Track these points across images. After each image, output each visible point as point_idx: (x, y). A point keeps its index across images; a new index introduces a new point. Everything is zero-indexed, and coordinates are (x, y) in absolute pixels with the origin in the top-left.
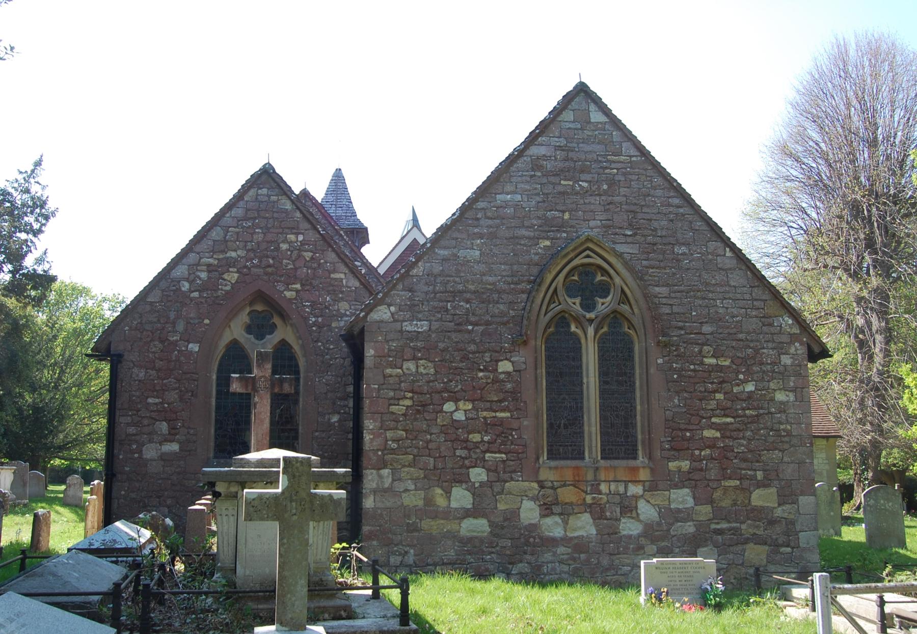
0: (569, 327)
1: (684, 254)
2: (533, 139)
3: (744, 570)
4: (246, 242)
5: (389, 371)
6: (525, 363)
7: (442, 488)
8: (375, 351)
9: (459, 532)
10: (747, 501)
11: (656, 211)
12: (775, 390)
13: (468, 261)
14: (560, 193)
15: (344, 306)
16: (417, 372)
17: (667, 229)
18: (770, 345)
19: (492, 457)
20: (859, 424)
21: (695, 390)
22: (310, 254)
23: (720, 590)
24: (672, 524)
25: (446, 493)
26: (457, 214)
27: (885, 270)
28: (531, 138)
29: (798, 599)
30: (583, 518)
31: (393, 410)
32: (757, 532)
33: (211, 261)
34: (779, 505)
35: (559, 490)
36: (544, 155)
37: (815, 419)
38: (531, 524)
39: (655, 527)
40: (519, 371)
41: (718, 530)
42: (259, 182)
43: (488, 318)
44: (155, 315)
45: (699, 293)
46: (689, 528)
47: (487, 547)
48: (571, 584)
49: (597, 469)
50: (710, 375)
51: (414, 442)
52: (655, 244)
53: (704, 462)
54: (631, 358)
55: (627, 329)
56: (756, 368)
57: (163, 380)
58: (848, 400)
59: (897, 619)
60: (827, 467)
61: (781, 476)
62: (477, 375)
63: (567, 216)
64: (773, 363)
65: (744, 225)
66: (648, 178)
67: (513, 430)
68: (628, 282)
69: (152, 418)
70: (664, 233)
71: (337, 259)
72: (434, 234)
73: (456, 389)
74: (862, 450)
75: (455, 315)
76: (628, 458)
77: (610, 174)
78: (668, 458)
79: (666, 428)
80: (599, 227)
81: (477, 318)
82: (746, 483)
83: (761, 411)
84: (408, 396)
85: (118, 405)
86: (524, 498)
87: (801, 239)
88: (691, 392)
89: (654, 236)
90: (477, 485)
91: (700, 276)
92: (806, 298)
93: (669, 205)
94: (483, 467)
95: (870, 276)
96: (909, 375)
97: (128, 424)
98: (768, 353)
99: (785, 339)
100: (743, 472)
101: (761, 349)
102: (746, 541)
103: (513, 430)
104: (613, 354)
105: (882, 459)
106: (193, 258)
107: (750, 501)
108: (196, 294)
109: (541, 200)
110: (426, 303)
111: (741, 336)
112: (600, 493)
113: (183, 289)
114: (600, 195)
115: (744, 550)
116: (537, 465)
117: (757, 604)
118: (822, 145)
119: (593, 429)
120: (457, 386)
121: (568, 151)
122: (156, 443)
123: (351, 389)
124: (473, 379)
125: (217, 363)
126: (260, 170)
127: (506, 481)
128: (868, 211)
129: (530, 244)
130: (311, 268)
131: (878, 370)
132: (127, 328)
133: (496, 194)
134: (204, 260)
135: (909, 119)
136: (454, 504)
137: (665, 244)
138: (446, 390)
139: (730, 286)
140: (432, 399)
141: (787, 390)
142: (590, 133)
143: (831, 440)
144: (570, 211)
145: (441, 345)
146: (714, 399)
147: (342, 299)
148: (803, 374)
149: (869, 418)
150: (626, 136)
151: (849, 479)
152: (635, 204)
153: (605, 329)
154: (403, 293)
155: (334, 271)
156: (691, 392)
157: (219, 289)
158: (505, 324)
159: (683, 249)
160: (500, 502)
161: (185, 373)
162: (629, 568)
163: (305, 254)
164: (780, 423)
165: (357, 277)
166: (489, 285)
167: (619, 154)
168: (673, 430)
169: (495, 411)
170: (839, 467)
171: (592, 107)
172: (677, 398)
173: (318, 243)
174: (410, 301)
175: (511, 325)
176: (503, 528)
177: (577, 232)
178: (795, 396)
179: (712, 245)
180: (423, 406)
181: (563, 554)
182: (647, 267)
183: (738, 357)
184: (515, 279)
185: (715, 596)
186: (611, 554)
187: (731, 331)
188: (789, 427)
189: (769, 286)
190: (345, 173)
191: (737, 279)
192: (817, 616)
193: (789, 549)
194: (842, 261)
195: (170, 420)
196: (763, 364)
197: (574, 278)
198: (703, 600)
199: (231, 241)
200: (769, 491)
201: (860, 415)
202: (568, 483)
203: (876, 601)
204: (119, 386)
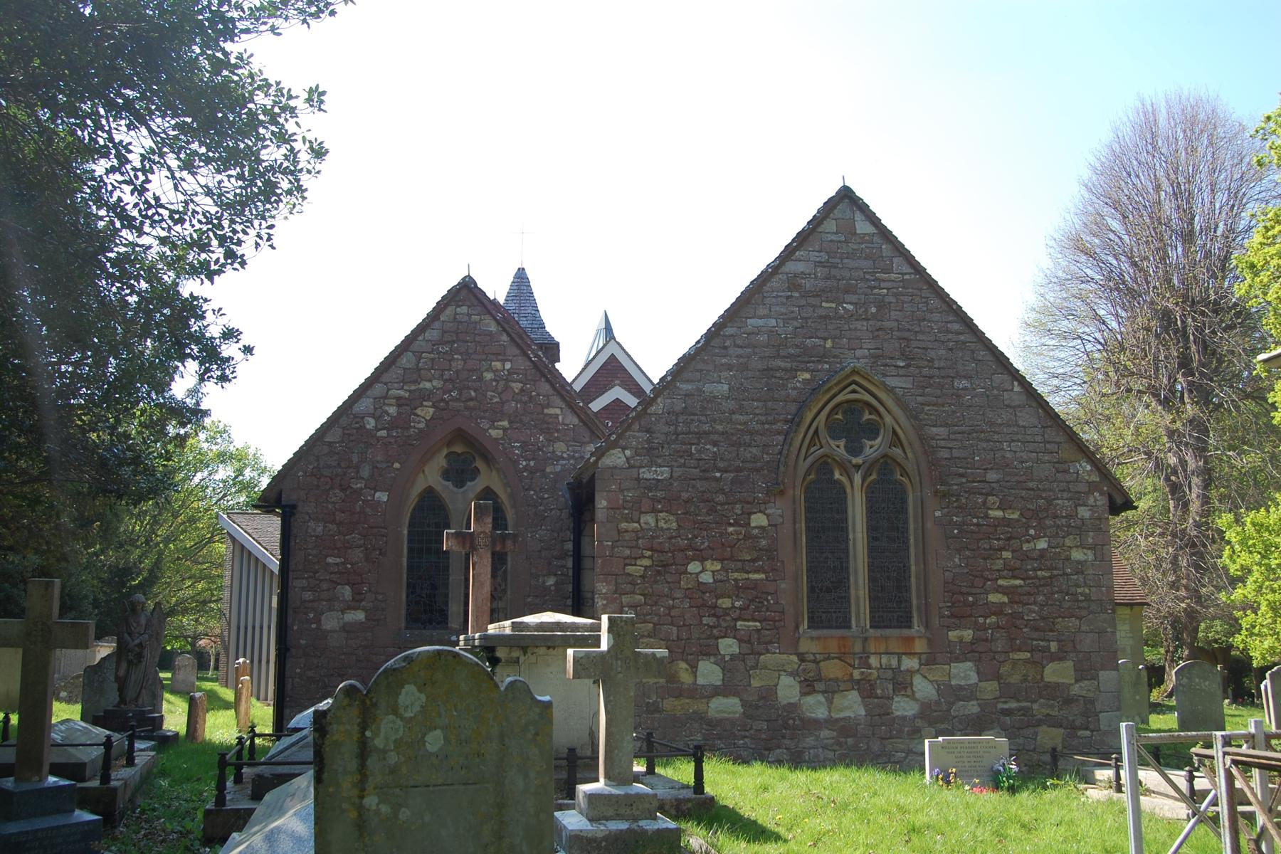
0: (832, 474)
1: (965, 389)
2: (790, 252)
3: (1035, 757)
4: (443, 370)
5: (624, 525)
6: (782, 516)
7: (687, 662)
8: (608, 502)
9: (707, 713)
10: (1039, 677)
11: (933, 338)
12: (1071, 548)
13: (714, 397)
14: (821, 317)
15: (560, 447)
16: (657, 526)
17: (946, 359)
18: (1065, 495)
19: (745, 625)
20: (1171, 588)
21: (978, 548)
22: (520, 385)
23: (1013, 771)
24: (953, 703)
25: (692, 667)
26: (702, 342)
27: (1203, 396)
28: (786, 253)
29: (1101, 781)
30: (850, 697)
31: (629, 571)
32: (1051, 713)
33: (401, 393)
34: (1077, 681)
35: (822, 664)
36: (802, 273)
37: (1118, 582)
38: (790, 704)
39: (933, 707)
40: (775, 525)
41: (1007, 709)
42: (457, 299)
43: (739, 463)
44: (334, 458)
45: (983, 435)
46: (973, 708)
47: (739, 731)
48: (847, 766)
49: (866, 640)
50: (996, 530)
51: (654, 609)
52: (931, 377)
53: (990, 631)
54: (904, 510)
55: (899, 477)
56: (1049, 522)
57: (344, 536)
58: (1157, 559)
59: (1196, 758)
60: (1131, 642)
61: (1078, 647)
62: (726, 529)
63: (829, 344)
64: (1069, 517)
65: (1027, 338)
66: (924, 300)
67: (768, 593)
68: (900, 421)
69: (333, 582)
70: (942, 364)
71: (551, 392)
72: (675, 364)
73: (702, 547)
74: (1175, 622)
75: (700, 459)
76: (900, 627)
77: (879, 294)
78: (948, 627)
79: (945, 592)
80: (866, 357)
81: (726, 463)
82: (1038, 656)
83: (1055, 572)
84: (647, 555)
85: (292, 566)
86: (782, 673)
87: (1097, 355)
88: (974, 550)
89: (930, 368)
90: (727, 658)
91: (983, 414)
92: (1104, 429)
93: (948, 331)
94: (735, 638)
95: (1184, 403)
96: (1231, 527)
97: (303, 589)
98: (1063, 504)
99: (1082, 487)
100: (1035, 643)
101: (1055, 499)
102: (1039, 723)
103: (768, 593)
104: (883, 505)
105: (1201, 635)
106: (378, 389)
107: (1042, 676)
108: (383, 433)
109: (799, 325)
110: (666, 446)
111: (1031, 485)
112: (869, 667)
113: (368, 427)
114: (867, 319)
115: (1036, 734)
116: (797, 634)
117: (1055, 786)
118: (1126, 238)
119: (861, 593)
120: (703, 543)
121: (830, 267)
122: (337, 611)
123: (569, 546)
124: (721, 535)
125: (409, 515)
126: (459, 284)
127: (761, 654)
128: (1183, 322)
129: (787, 377)
130: (520, 401)
131: (1195, 521)
132: (301, 473)
133: (747, 318)
134: (393, 392)
135: (1233, 206)
136: (701, 681)
137: (943, 377)
138: (690, 548)
139: (1019, 426)
140: (674, 559)
141: (1085, 548)
142: (855, 247)
143: (1136, 608)
144: (833, 338)
145: (685, 495)
146: (1001, 558)
147: (558, 438)
148: (1104, 529)
149: (1184, 582)
150: (898, 250)
151: (1160, 659)
152: (909, 330)
153: (874, 476)
154: (640, 434)
155: (548, 406)
156: (974, 550)
157: (410, 426)
158: (758, 470)
159: (965, 383)
160: (754, 678)
161: (372, 527)
162: (904, 754)
163: (513, 385)
164: (1078, 586)
165: (576, 413)
166: (740, 424)
167: (889, 271)
168: (953, 594)
169: (748, 572)
170: (1146, 644)
171: (858, 216)
172: (958, 556)
173: (529, 371)
174: (648, 443)
175: (766, 471)
176: (757, 707)
177: (841, 363)
178: (1095, 554)
179: (998, 378)
180: (663, 566)
181: (827, 739)
182: (922, 404)
183: (1029, 509)
184: (770, 418)
185: (1008, 778)
186: (883, 739)
187: (1021, 479)
188: (1087, 591)
189: (1063, 426)
190: (530, 274)
191: (1027, 418)
192: (1126, 797)
193: (1088, 732)
194: (1150, 384)
195: (354, 584)
196: (1057, 517)
197: (837, 416)
198: (995, 781)
199: (426, 369)
200: (1065, 665)
201: (1172, 578)
202: (832, 655)
203: (1185, 777)
204: (292, 544)
